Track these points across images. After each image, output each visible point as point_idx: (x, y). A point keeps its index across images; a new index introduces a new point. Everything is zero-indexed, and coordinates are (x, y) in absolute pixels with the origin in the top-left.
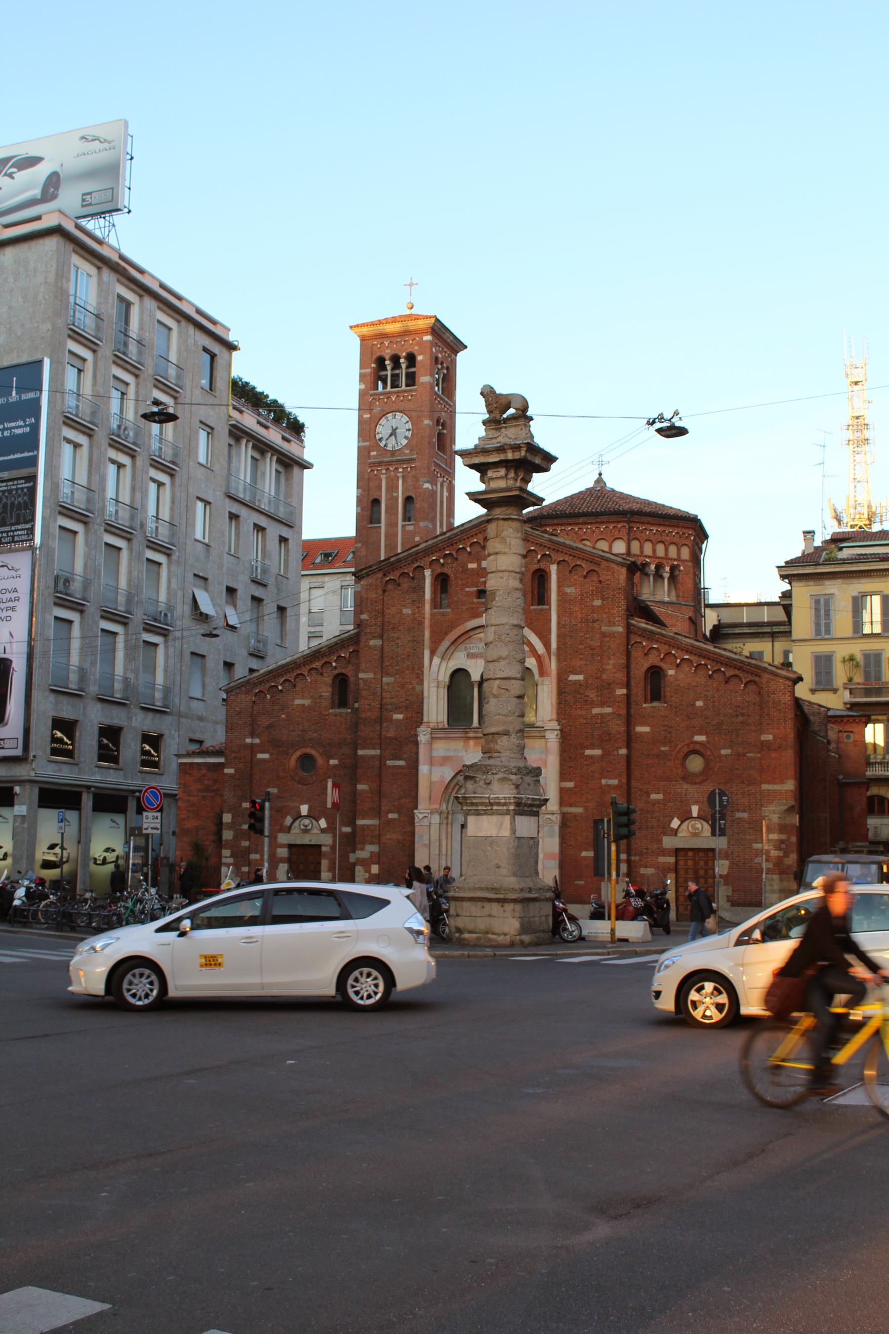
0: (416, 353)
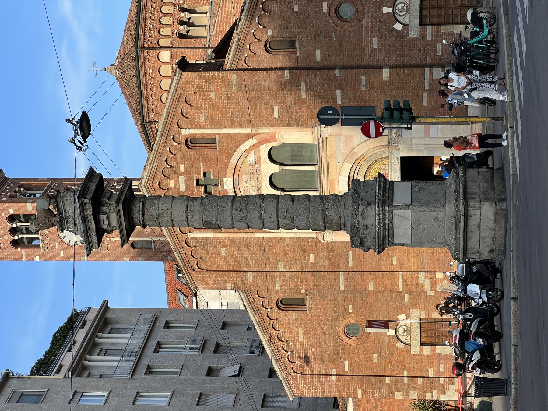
0: (8, 214)
